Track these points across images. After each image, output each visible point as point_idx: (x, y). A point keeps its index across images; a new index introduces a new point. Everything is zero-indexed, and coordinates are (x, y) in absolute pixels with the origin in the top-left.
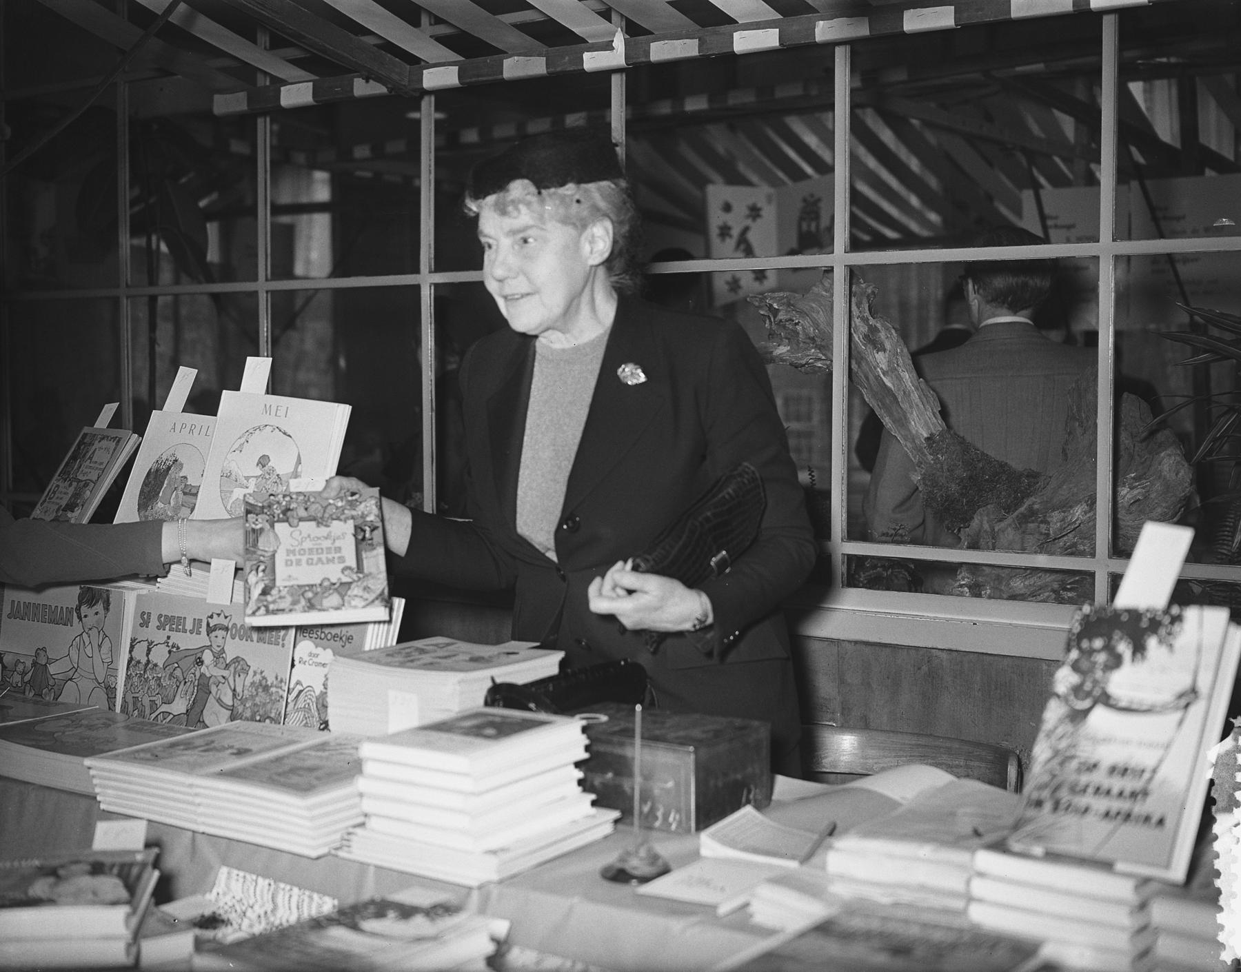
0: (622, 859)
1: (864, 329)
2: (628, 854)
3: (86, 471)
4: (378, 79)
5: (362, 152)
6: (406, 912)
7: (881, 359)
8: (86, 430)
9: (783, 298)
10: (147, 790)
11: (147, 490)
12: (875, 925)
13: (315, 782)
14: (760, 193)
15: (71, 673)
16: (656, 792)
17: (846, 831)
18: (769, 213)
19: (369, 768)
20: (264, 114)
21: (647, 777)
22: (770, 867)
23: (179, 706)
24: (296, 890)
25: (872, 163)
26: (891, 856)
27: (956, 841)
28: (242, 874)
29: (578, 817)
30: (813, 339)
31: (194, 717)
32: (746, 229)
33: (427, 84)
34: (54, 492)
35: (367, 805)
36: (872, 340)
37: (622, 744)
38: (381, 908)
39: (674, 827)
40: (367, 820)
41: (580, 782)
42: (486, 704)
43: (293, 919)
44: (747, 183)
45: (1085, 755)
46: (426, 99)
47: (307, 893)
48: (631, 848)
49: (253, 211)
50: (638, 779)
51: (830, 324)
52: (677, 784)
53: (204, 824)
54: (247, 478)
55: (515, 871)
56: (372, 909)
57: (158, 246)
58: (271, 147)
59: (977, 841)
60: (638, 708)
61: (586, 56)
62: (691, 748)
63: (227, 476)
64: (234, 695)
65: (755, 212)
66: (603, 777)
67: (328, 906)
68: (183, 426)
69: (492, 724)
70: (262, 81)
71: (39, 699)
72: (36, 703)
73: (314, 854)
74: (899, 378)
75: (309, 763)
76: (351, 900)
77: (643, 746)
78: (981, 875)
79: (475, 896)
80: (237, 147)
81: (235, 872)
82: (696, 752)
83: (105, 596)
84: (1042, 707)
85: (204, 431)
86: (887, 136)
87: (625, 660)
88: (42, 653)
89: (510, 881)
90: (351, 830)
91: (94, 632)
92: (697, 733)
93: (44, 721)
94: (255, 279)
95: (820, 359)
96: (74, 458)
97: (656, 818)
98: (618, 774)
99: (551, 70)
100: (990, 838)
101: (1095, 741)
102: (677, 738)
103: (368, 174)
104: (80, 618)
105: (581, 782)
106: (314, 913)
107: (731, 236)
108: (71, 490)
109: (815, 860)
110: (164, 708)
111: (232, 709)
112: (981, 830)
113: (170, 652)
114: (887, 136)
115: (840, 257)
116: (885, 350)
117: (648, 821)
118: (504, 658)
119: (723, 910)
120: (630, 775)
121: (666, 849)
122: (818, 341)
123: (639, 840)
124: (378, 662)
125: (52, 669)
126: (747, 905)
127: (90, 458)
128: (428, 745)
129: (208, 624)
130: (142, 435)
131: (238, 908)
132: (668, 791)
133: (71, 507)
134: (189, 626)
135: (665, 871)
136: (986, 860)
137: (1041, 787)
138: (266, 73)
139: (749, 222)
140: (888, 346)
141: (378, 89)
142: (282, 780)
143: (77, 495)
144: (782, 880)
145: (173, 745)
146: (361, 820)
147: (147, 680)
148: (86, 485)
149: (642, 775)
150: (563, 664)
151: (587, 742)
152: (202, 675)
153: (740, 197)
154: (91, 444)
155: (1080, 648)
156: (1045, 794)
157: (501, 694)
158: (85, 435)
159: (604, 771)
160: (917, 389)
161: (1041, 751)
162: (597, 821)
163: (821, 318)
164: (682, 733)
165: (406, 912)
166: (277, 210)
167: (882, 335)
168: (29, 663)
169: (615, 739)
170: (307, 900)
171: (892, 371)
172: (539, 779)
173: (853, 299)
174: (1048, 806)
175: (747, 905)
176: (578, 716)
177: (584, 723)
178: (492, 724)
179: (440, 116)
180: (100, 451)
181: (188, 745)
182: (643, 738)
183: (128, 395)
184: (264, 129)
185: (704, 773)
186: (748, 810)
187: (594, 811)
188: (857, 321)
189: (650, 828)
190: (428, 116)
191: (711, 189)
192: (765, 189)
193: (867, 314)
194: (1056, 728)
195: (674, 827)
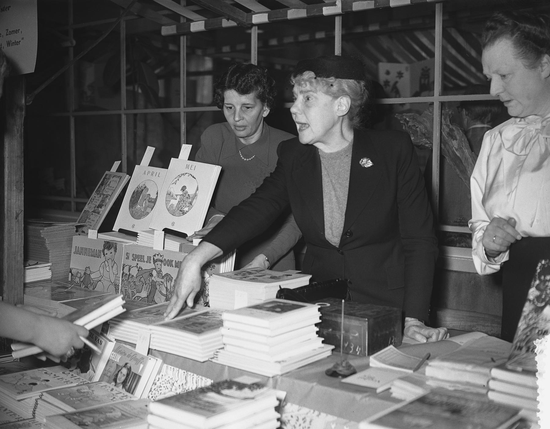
0: (335, 367)
1: (447, 130)
2: (337, 364)
3: (107, 191)
4: (233, 20)
5: (226, 49)
6: (241, 386)
7: (455, 143)
8: (107, 172)
9: (411, 116)
10: (132, 331)
11: (133, 199)
12: (445, 399)
13: (203, 329)
14: (402, 67)
15: (100, 278)
16: (351, 338)
17: (434, 358)
18: (407, 76)
19: (225, 324)
20: (183, 35)
21: (347, 331)
22: (401, 372)
23: (144, 294)
24: (195, 375)
25: (453, 52)
26: (453, 369)
27: (483, 364)
28: (172, 367)
29: (316, 348)
30: (424, 134)
31: (150, 299)
32: (396, 82)
33: (254, 21)
34: (93, 199)
35: (225, 340)
36: (451, 135)
37: (336, 317)
38: (230, 384)
39: (358, 353)
40: (225, 346)
41: (317, 333)
42: (277, 297)
43: (194, 388)
44: (397, 62)
45: (542, 327)
46: (254, 28)
47: (200, 377)
48: (339, 362)
49: (177, 75)
50: (343, 332)
51: (432, 128)
52: (360, 335)
53: (155, 346)
54: (177, 195)
55: (288, 371)
56: (226, 385)
57: (138, 90)
58: (187, 46)
59: (493, 364)
60: (343, 301)
61: (324, 8)
62: (367, 319)
63: (169, 194)
64: (167, 290)
65: (400, 75)
66: (327, 330)
67: (208, 382)
68: (149, 172)
69: (279, 306)
70: (182, 20)
71: (86, 289)
72: (85, 291)
73: (202, 361)
74: (463, 152)
75: (201, 321)
76: (219, 380)
77: (344, 317)
78: (494, 379)
79: (271, 381)
80: (172, 47)
81: (170, 366)
82: (368, 321)
83: (114, 245)
84: (523, 306)
85: (157, 175)
86: (461, 40)
87: (338, 280)
88: (88, 269)
89: (287, 374)
90: (218, 350)
91: (110, 261)
92: (369, 312)
93: (88, 299)
94: (179, 107)
95: (427, 143)
96: (102, 184)
97: (351, 349)
98: (333, 329)
99: (309, 15)
100: (498, 362)
101: (546, 320)
102: (361, 314)
103: (228, 59)
104: (104, 255)
105: (317, 333)
106: (203, 386)
107: (389, 85)
108: (101, 199)
109: (420, 370)
110: (138, 295)
111: (166, 296)
112: (495, 359)
113: (138, 270)
114: (461, 40)
115: (436, 97)
116: (456, 140)
117: (347, 351)
118: (285, 277)
119: (379, 391)
120: (340, 330)
121: (355, 363)
122: (427, 135)
123: (343, 359)
124: (231, 277)
125: (92, 276)
126: (390, 389)
127: (109, 185)
128: (252, 315)
129: (154, 259)
130: (131, 175)
131: (170, 381)
132: (356, 337)
133: (100, 206)
134: (146, 259)
135: (354, 373)
136: (496, 373)
137: (521, 341)
138: (184, 17)
139: (398, 79)
140: (458, 138)
141: (232, 24)
142: (189, 328)
143: (103, 201)
144: (406, 379)
145: (142, 312)
146: (222, 346)
147: (129, 282)
148: (107, 197)
149: (345, 330)
150: (311, 280)
151: (321, 315)
152: (153, 280)
153: (394, 68)
154: (109, 179)
155: (540, 279)
156: (523, 344)
157: (283, 293)
158: (107, 175)
159: (328, 328)
160: (471, 157)
161: (522, 325)
162: (324, 350)
163: (428, 125)
164: (362, 312)
165: (241, 386)
166: (189, 74)
167: (456, 133)
168: (82, 274)
169: (333, 314)
170: (200, 380)
171: (460, 149)
172: (299, 334)
173: (443, 117)
174: (524, 350)
175: (390, 389)
176: (317, 304)
177: (319, 307)
178: (279, 306)
179: (260, 31)
180: (113, 182)
181: (149, 312)
182: (344, 314)
183: (124, 157)
184: (183, 40)
185: (372, 331)
186: (391, 347)
187: (323, 345)
188: (444, 126)
189: (348, 354)
190: (254, 33)
191: (380, 64)
192: (405, 65)
193: (449, 123)
194: (528, 314)
195: (358, 353)
